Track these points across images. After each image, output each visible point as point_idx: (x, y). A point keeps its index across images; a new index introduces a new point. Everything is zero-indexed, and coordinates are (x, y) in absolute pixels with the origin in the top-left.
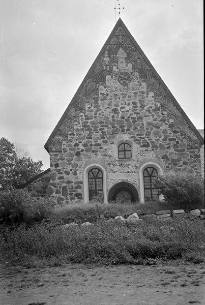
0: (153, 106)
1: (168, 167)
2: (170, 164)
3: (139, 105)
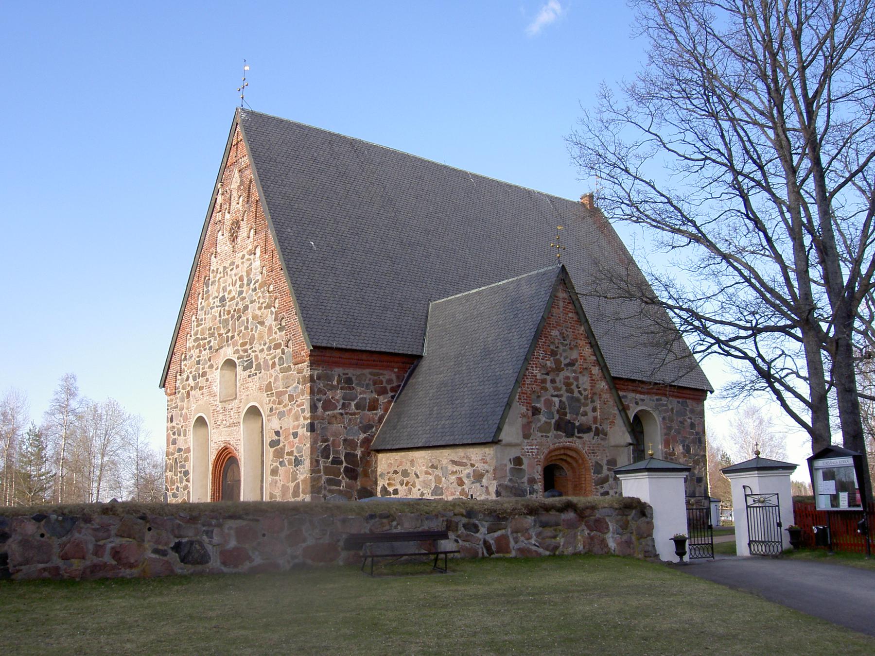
0: (259, 277)
1: (271, 410)
2: (274, 402)
3: (245, 282)
